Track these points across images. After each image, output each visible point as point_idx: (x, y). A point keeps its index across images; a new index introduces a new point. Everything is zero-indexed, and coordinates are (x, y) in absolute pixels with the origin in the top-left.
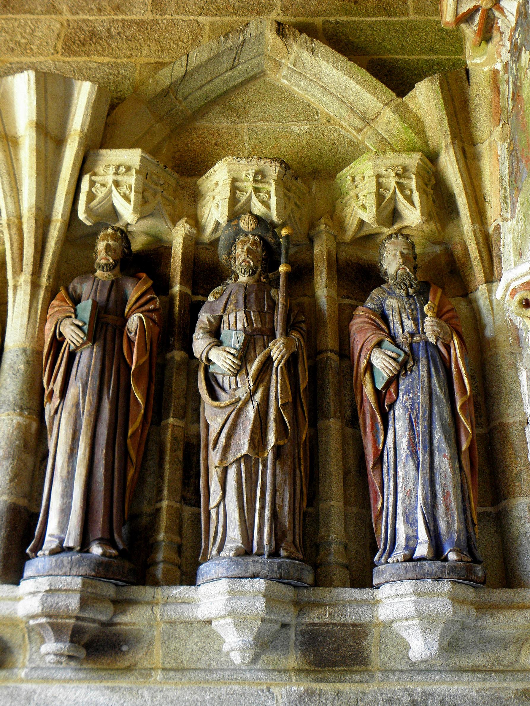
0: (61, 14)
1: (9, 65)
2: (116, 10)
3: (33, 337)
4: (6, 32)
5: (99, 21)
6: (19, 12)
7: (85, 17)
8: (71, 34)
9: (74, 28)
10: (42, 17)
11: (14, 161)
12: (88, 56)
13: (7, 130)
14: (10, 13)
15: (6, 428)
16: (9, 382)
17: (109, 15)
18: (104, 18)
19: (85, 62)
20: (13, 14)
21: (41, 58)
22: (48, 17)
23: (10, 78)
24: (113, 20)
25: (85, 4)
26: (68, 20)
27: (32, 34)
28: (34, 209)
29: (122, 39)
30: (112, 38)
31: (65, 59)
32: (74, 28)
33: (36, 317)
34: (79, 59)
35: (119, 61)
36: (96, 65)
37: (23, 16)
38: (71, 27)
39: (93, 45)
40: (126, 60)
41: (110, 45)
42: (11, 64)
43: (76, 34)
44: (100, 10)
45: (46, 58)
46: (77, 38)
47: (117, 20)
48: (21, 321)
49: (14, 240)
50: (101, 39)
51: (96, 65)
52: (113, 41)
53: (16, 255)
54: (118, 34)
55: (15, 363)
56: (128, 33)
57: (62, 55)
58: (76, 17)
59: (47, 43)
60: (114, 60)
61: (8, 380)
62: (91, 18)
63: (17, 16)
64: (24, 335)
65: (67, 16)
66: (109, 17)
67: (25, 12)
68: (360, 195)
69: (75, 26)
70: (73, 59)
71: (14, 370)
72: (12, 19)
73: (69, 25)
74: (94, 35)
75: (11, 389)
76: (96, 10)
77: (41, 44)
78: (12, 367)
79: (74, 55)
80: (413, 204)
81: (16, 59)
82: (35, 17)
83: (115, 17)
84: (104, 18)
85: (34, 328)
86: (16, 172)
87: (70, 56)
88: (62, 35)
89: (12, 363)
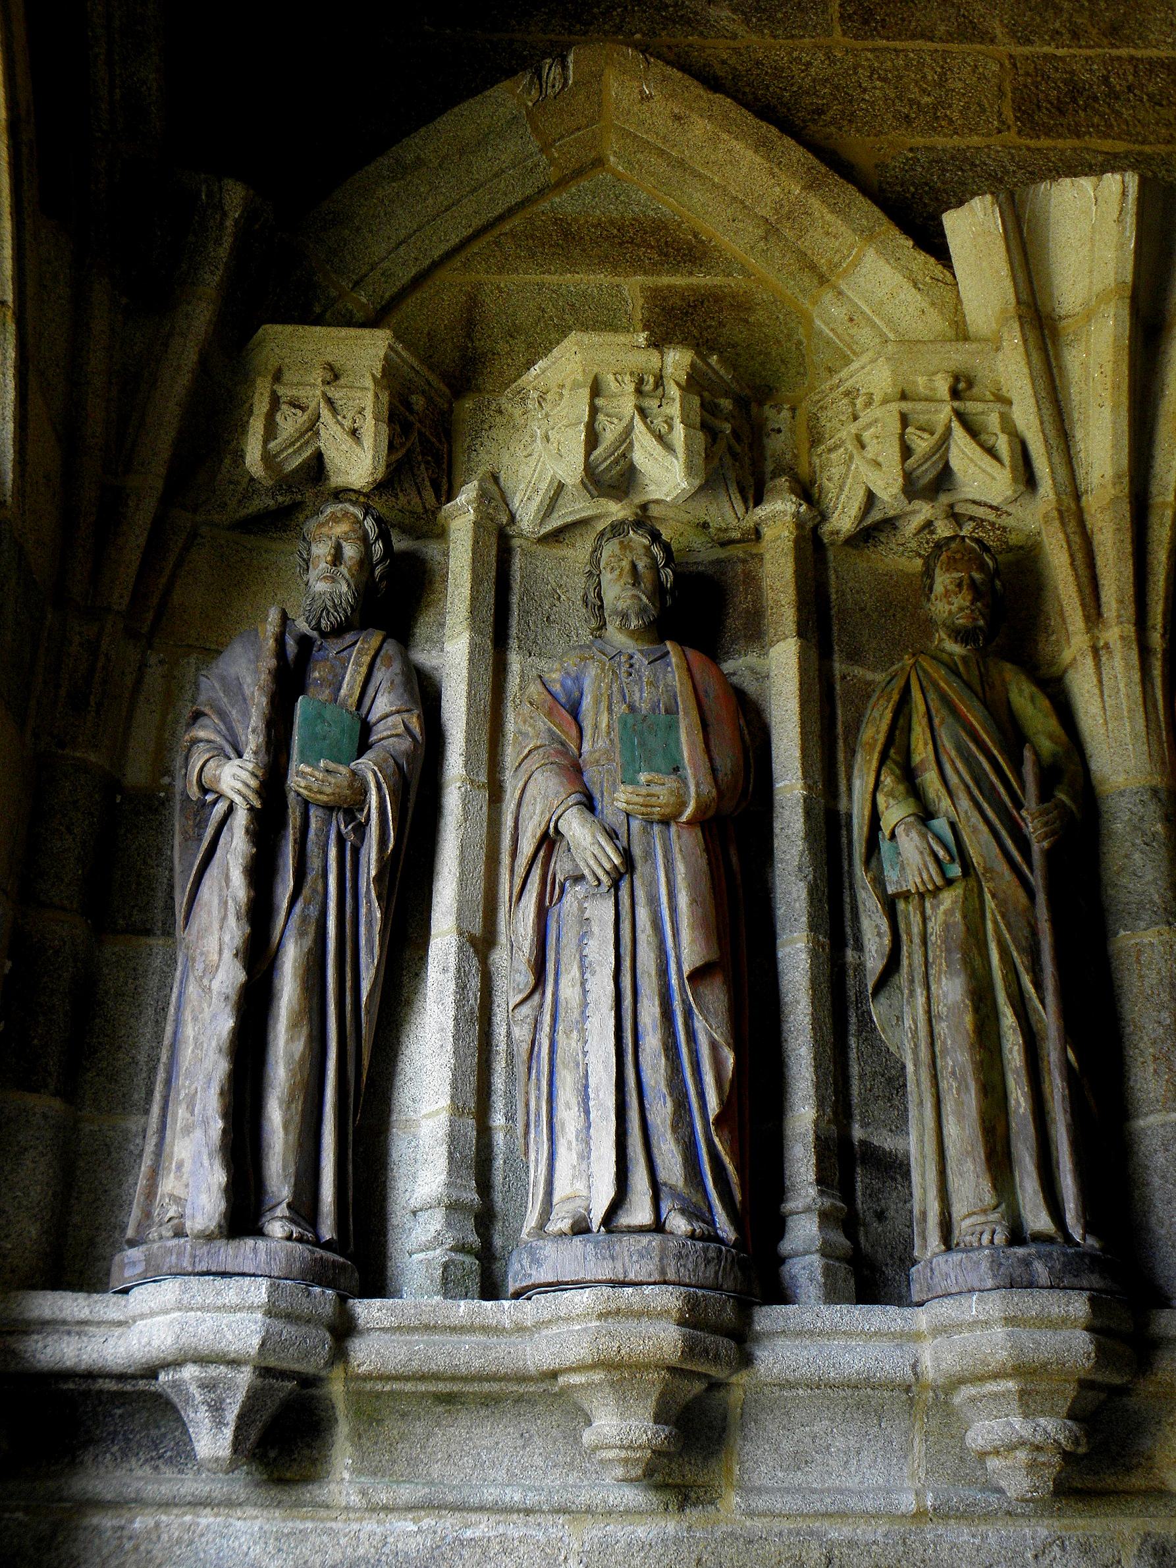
0: (992, 41)
1: (911, 155)
2: (1111, 34)
3: (1163, 763)
4: (884, 80)
5: (1085, 58)
6: (898, 36)
7: (1046, 49)
8: (1026, 86)
9: (1028, 74)
10: (954, 47)
11: (1055, 370)
12: (1078, 137)
13: (1039, 303)
14: (882, 38)
15: (1162, 964)
16: (1140, 863)
17: (1100, 46)
18: (1089, 52)
19: (1074, 149)
20: (888, 39)
21: (976, 140)
22: (966, 47)
23: (1044, 186)
24: (1112, 59)
25: (1038, 19)
26: (1011, 56)
27: (941, 82)
28: (1126, 480)
29: (1141, 100)
30: (1117, 98)
31: (1032, 143)
32: (1028, 74)
33: (1158, 717)
34: (1060, 143)
35: (1147, 149)
36: (1100, 158)
37: (909, 44)
38: (1021, 72)
39: (1082, 114)
40: (1162, 147)
41: (1118, 114)
42: (911, 150)
43: (1037, 87)
44: (1075, 36)
45: (989, 141)
46: (1041, 96)
47: (1119, 58)
48: (1133, 728)
49: (1075, 547)
50: (1096, 99)
51: (1100, 158)
52: (1123, 106)
53: (1084, 580)
54: (1130, 89)
55: (1142, 819)
56: (1151, 88)
57: (1019, 133)
58: (1027, 50)
59: (979, 105)
60: (1137, 147)
61: (1137, 856)
62: (1061, 52)
63: (898, 44)
64: (1146, 756)
65: (1007, 47)
66: (1099, 50)
67: (913, 37)
68: (867, 436)
69: (1031, 69)
70: (1045, 142)
71: (1144, 834)
72: (887, 49)
73: (1015, 65)
74: (1075, 89)
75: (1150, 878)
76: (1067, 36)
77: (967, 107)
78: (1136, 828)
79: (1047, 135)
80: (669, 447)
81: (919, 141)
82: (939, 46)
83: (1115, 52)
84: (1089, 52)
85: (1161, 743)
86: (1060, 396)
87: (1038, 137)
88: (1008, 87)
89: (1136, 820)
